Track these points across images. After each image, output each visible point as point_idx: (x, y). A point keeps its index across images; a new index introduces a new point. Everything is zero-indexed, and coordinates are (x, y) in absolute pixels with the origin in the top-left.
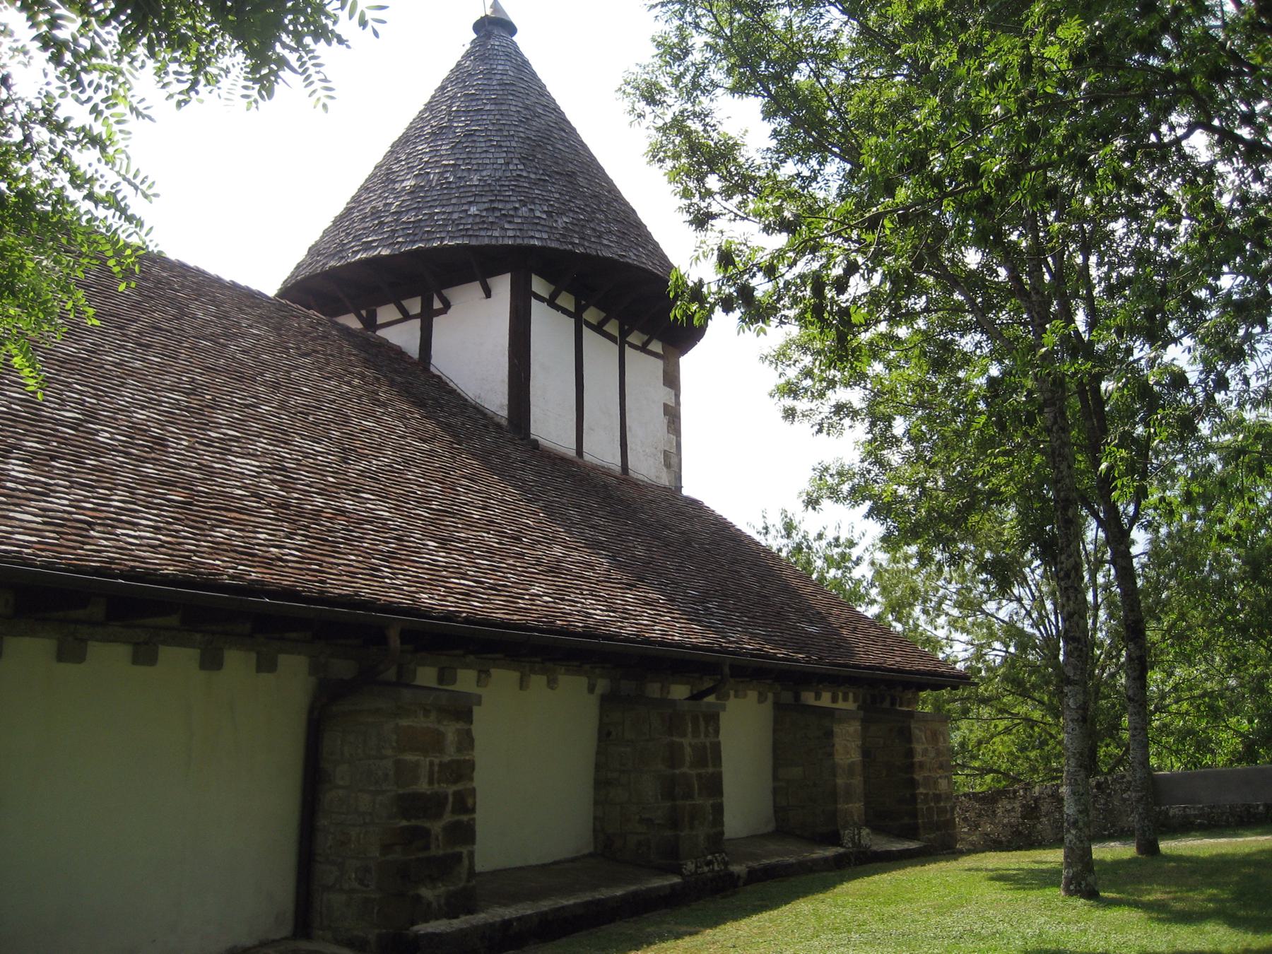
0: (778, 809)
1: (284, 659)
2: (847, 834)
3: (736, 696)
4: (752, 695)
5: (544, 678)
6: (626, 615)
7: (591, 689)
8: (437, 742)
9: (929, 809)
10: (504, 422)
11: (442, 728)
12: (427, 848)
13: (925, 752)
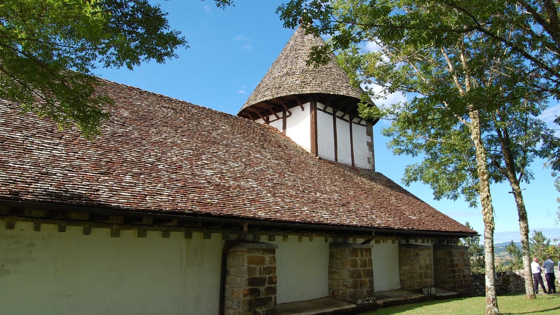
0: (401, 281)
1: (213, 235)
2: (425, 290)
3: (383, 242)
5: (308, 238)
7: (326, 241)
8: (262, 261)
10: (309, 151)
11: (264, 256)
12: (259, 295)
13: (458, 260)
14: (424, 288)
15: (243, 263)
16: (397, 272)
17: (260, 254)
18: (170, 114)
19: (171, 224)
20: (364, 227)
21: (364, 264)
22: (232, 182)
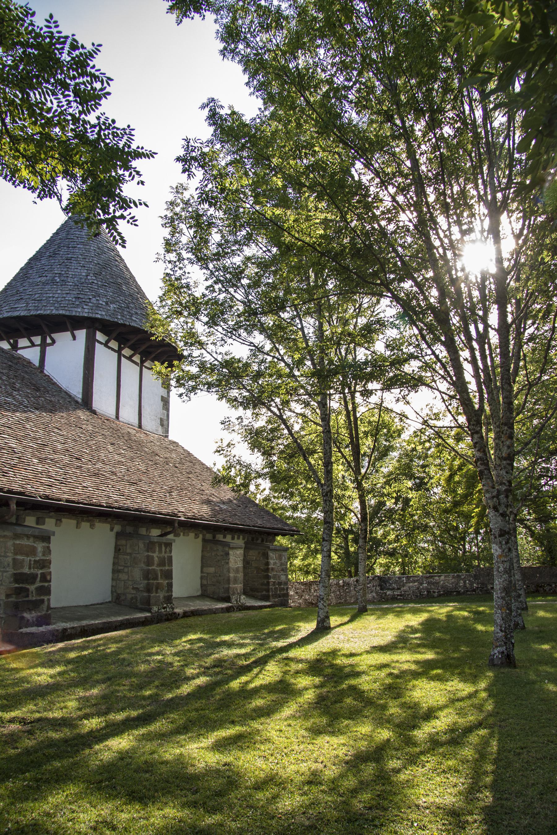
0: (202, 585)
4: (192, 535)
5: (88, 524)
6: (128, 497)
7: (112, 529)
8: (33, 551)
9: (276, 588)
10: (80, 400)
12: (28, 596)
13: (275, 564)
15: (5, 552)
16: (199, 574)
17: (29, 542)
21: (162, 563)
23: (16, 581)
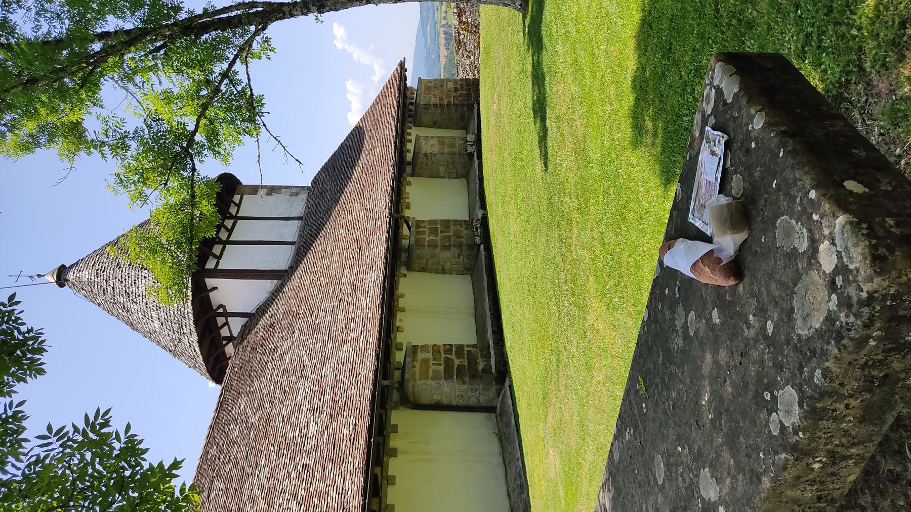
7: (405, 276)
8: (425, 362)
10: (280, 282)
14: (466, 150)
17: (417, 364)
18: (222, 486)
19: (379, 475)
20: (389, 228)
21: (434, 231)
22: (327, 397)
23: (451, 377)
